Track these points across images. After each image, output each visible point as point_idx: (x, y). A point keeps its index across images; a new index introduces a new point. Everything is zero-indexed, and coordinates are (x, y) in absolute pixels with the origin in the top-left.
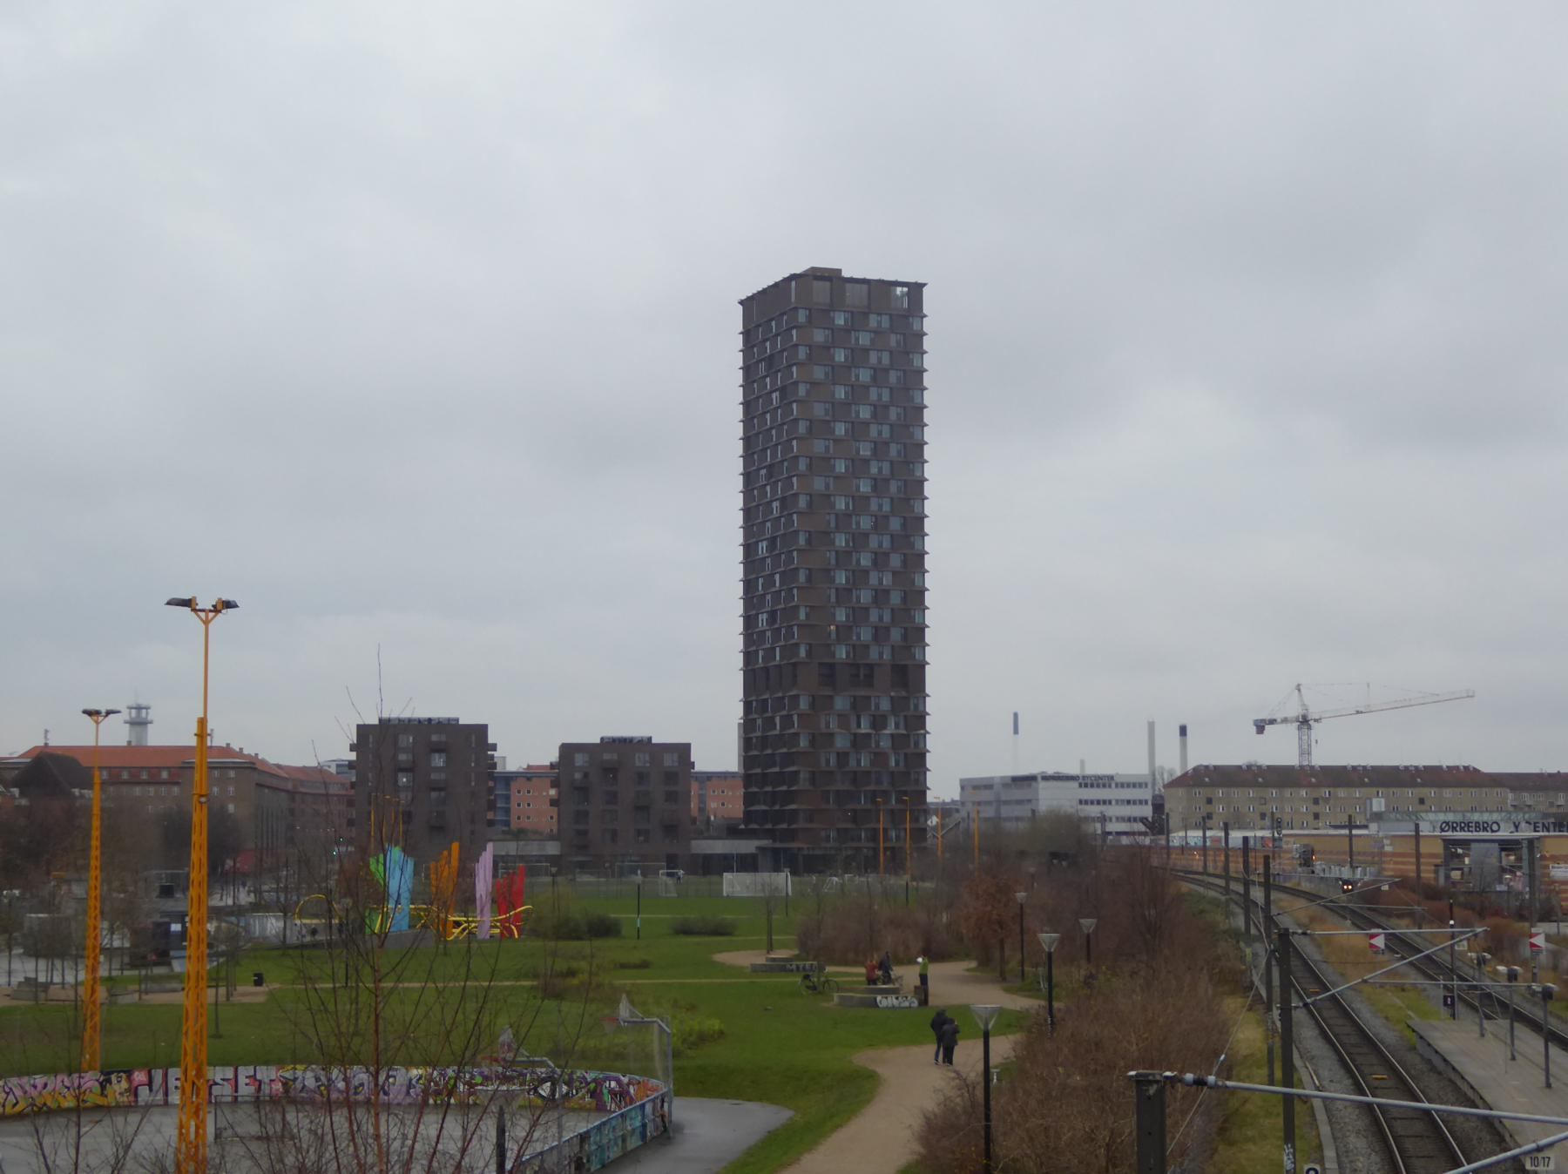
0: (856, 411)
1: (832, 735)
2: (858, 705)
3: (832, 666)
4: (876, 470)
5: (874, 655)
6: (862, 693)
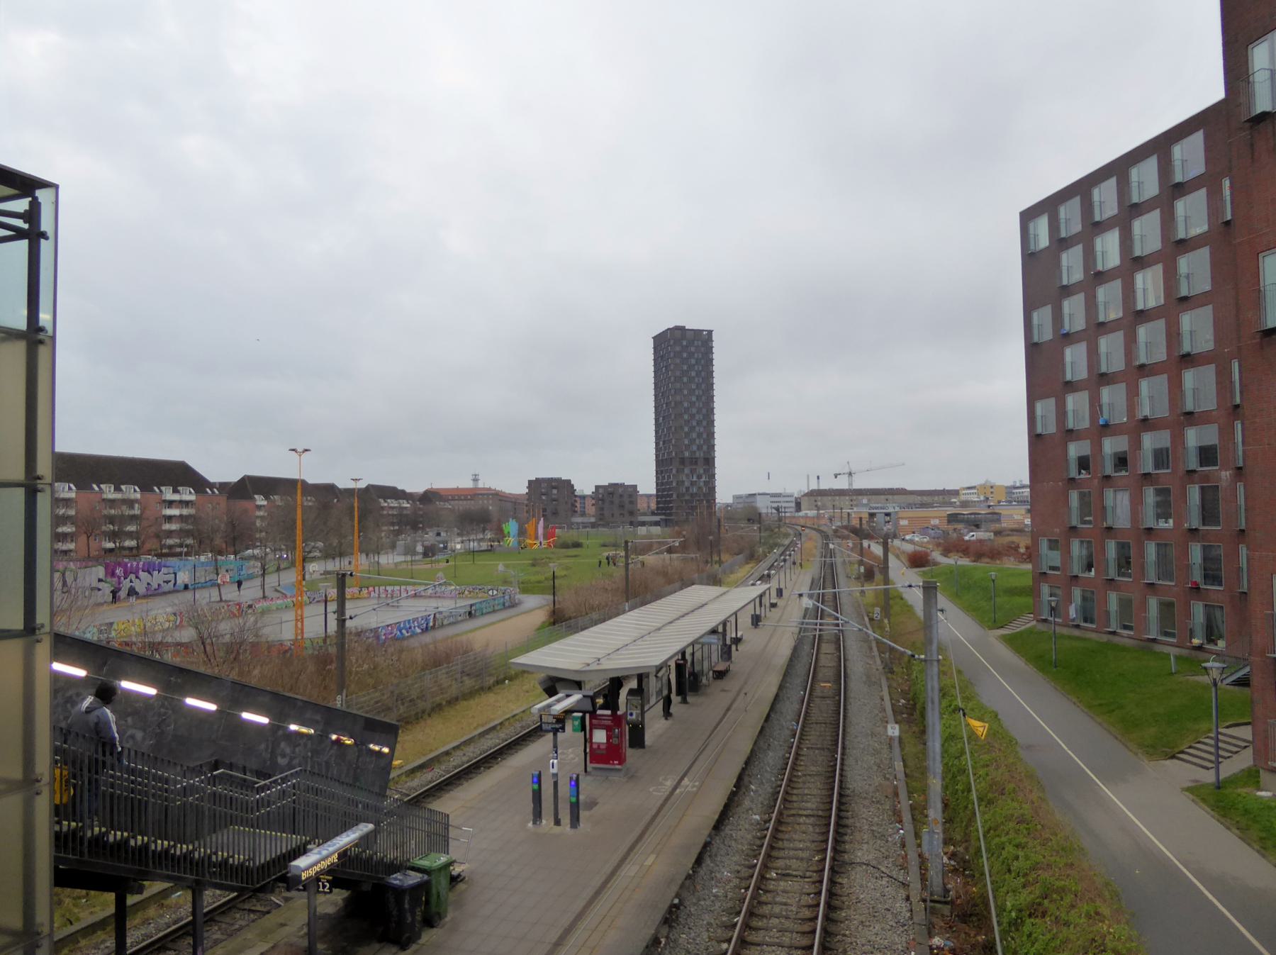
6: (694, 467)
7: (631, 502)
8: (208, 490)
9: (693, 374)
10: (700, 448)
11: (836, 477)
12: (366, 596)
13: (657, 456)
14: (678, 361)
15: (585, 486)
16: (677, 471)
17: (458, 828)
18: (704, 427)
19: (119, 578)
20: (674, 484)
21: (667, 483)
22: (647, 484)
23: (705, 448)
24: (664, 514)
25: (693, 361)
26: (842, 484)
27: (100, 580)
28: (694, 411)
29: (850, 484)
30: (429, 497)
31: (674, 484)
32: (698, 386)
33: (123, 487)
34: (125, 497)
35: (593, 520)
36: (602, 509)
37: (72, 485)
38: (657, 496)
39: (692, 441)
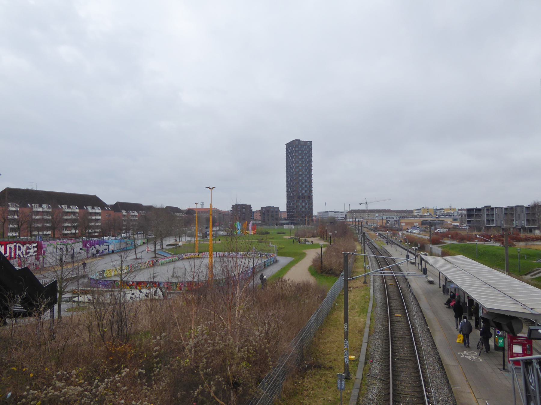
7: (276, 215)
8: (106, 208)
9: (303, 160)
10: (306, 191)
11: (360, 204)
12: (201, 256)
13: (287, 195)
14: (297, 154)
15: (256, 208)
16: (296, 202)
18: (308, 183)
19: (88, 247)
20: (295, 207)
21: (292, 207)
22: (283, 208)
23: (308, 192)
24: (290, 220)
25: (303, 154)
26: (363, 207)
27: (81, 249)
28: (304, 176)
29: (367, 207)
30: (190, 212)
31: (295, 207)
32: (306, 165)
33: (71, 207)
34: (73, 211)
35: (260, 222)
36: (264, 217)
37: (77, 207)
38: (287, 212)
39: (303, 189)
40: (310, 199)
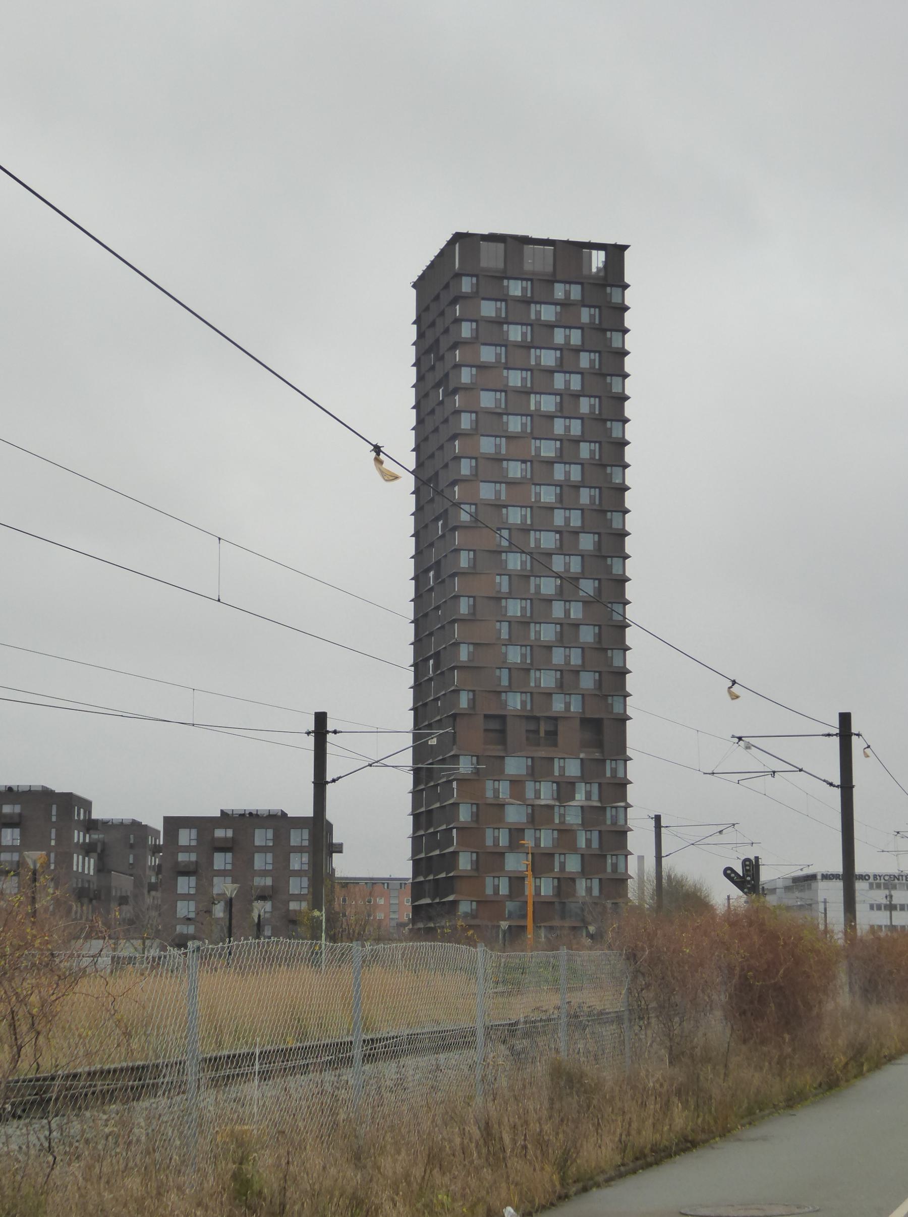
0: (536, 357)
1: (502, 806)
2: (537, 772)
3: (502, 718)
4: (563, 706)
5: (558, 705)
6: (542, 753)
17: (4, 1128)
38: (417, 889)
40: (599, 744)
